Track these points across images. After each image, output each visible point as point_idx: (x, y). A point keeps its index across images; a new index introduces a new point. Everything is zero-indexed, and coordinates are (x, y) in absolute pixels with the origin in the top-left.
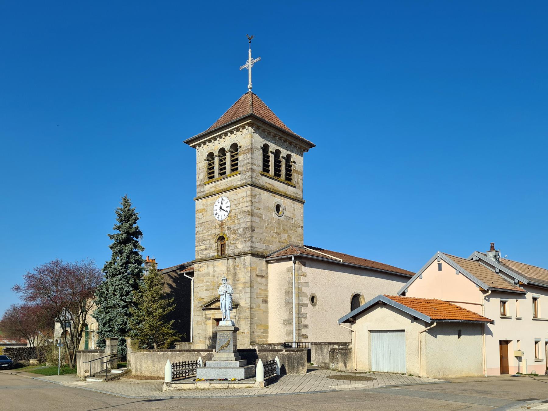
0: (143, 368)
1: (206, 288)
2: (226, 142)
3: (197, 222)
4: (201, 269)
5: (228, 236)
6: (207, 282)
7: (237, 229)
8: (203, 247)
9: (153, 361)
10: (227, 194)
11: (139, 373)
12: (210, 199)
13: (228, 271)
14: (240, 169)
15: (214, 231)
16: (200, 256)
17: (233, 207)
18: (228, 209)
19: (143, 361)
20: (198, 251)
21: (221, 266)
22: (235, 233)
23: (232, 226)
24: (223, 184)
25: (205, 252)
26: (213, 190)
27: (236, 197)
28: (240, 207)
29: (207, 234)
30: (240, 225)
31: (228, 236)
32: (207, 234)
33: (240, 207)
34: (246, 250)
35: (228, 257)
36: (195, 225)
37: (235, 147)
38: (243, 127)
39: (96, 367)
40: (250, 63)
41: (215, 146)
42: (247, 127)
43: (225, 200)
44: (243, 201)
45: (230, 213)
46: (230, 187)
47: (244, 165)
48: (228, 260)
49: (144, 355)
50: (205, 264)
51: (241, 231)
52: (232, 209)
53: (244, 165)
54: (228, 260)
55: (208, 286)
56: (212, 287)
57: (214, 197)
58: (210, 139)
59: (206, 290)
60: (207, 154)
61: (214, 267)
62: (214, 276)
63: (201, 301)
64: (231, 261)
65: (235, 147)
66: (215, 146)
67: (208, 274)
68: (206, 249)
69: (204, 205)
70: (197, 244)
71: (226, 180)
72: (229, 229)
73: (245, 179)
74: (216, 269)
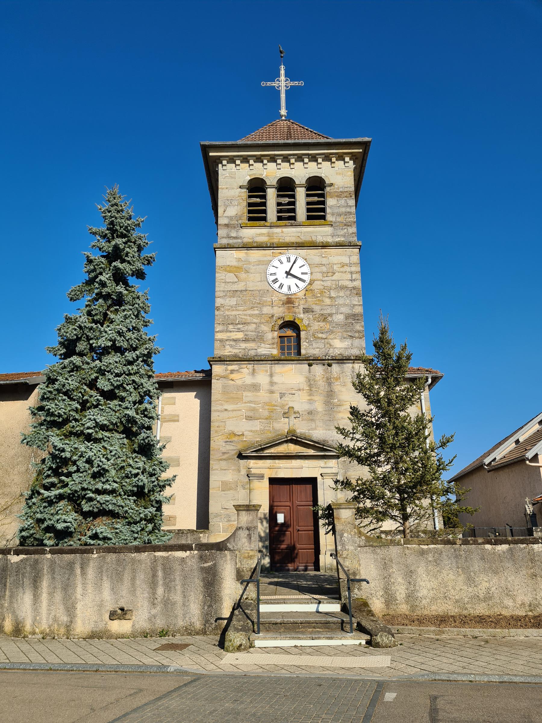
0: (423, 592)
1: (251, 414)
2: (300, 172)
3: (220, 287)
4: (232, 376)
5: (306, 322)
6: (250, 402)
7: (330, 315)
8: (240, 335)
9: (466, 570)
10: (303, 252)
11: (404, 608)
12: (256, 255)
13: (310, 386)
14: (329, 218)
15: (267, 310)
16: (228, 351)
17: (319, 276)
18: (307, 278)
19: (421, 570)
20: (221, 341)
21: (291, 375)
22: (325, 320)
23: (317, 308)
24: (289, 233)
25: (243, 345)
26: (263, 239)
27: (324, 261)
28: (334, 278)
29: (249, 312)
30: (338, 309)
31: (306, 322)
32: (249, 312)
33: (334, 278)
34: (355, 352)
35: (311, 361)
36: (214, 291)
37: (316, 185)
38: (341, 157)
39: (177, 597)
40: (282, 83)
41: (271, 172)
42: (347, 159)
43: (301, 263)
44: (342, 269)
45: (310, 284)
46: (313, 242)
47: (340, 215)
48: (310, 365)
49: (422, 553)
50: (246, 369)
51: (340, 318)
52: (314, 277)
53: (340, 215)
54: (310, 365)
55: (254, 410)
56: (266, 413)
57: (269, 252)
58: (291, 155)
59: (249, 418)
60: (249, 178)
61: (271, 375)
62: (272, 392)
63: (236, 439)
64: (318, 369)
65: (316, 185)
66: (271, 172)
67: (255, 387)
68: (246, 340)
69: (239, 260)
70: (218, 328)
71: (299, 229)
72: (306, 310)
73: (344, 236)
74: (275, 379)
